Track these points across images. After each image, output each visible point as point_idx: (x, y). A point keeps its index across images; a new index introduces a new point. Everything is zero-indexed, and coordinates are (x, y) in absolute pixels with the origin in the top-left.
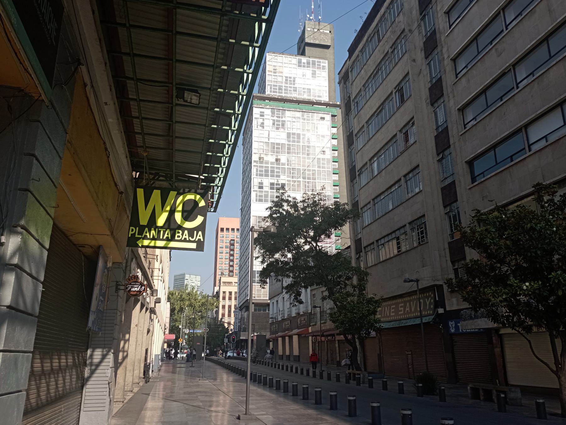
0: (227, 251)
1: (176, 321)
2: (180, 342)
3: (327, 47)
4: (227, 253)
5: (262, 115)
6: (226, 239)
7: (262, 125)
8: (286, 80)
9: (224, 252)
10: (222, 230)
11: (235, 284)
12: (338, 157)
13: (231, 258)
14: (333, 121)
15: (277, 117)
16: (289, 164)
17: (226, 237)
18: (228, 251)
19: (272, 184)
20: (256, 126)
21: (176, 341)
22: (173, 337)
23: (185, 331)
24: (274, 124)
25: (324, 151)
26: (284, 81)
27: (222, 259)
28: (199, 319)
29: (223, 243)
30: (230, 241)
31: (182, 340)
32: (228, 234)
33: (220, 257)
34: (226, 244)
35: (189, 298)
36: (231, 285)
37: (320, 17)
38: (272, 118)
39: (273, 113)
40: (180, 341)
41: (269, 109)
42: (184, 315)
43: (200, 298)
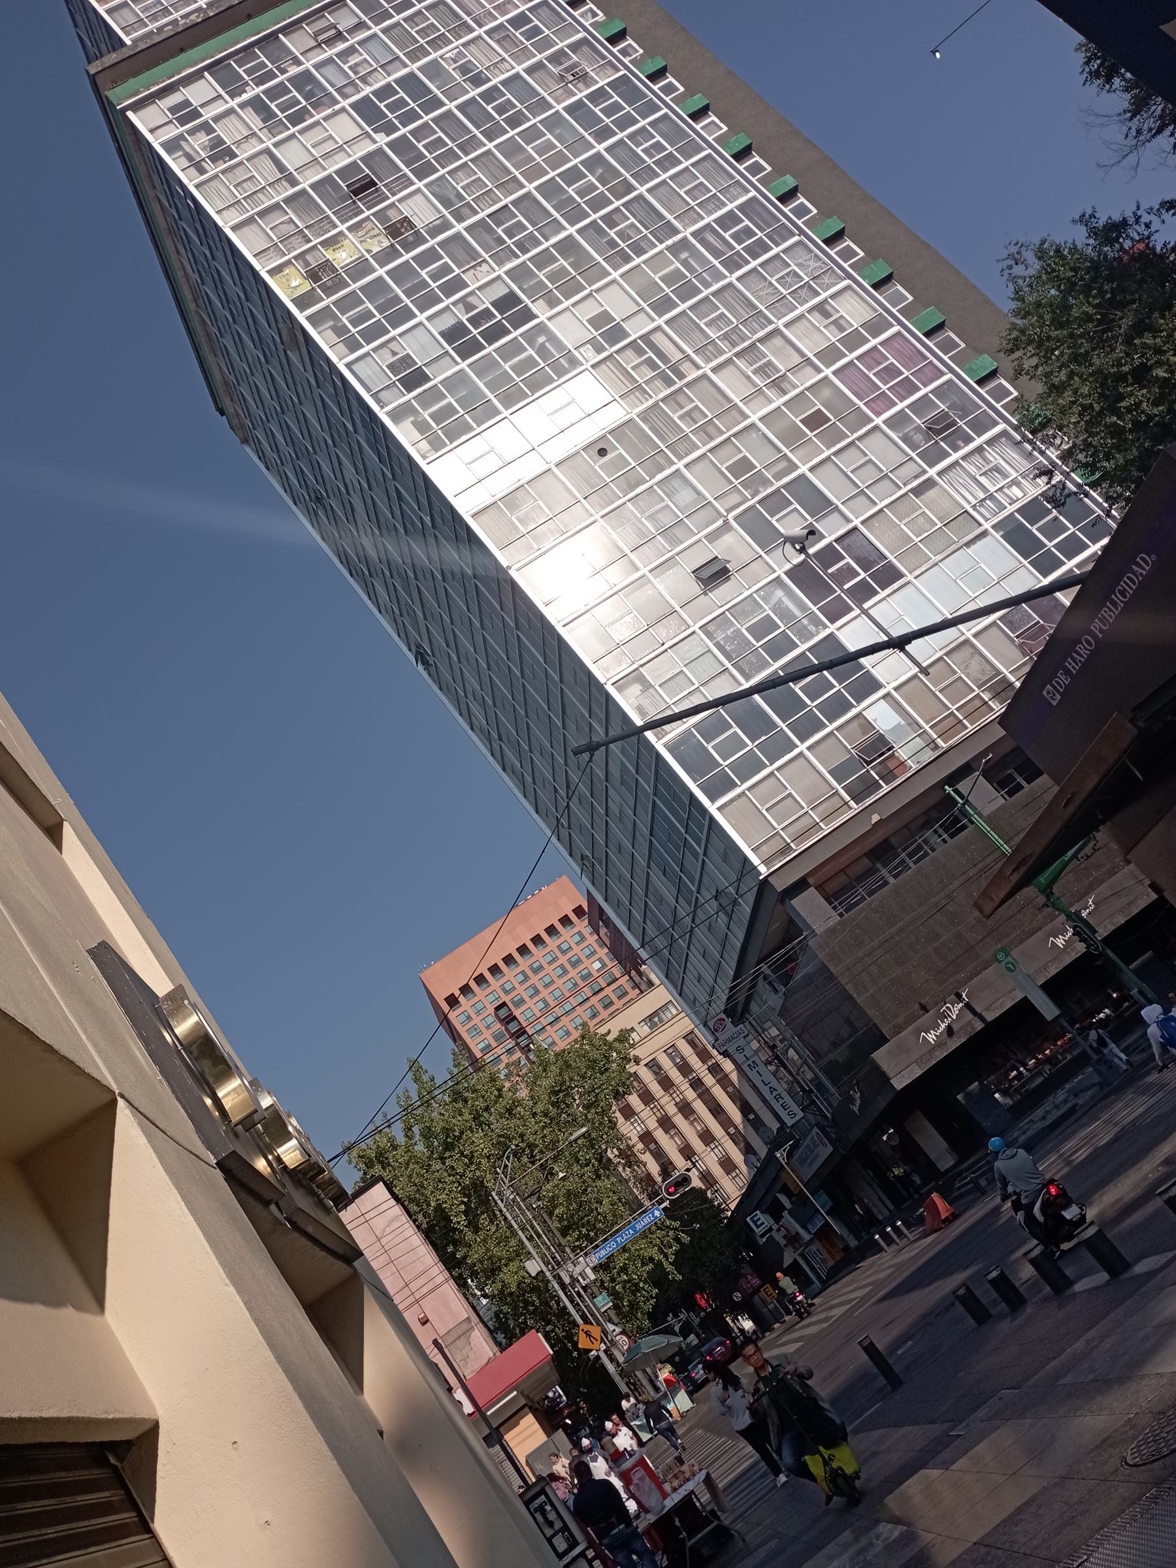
2: (598, 1350)
5: (186, 114)
6: (481, 1017)
7: (221, 152)
10: (452, 1001)
15: (259, 82)
17: (478, 1013)
19: (453, 334)
29: (480, 1033)
30: (496, 1015)
31: (596, 1331)
34: (491, 1031)
39: (233, 86)
40: (590, 1342)
42: (507, 1193)
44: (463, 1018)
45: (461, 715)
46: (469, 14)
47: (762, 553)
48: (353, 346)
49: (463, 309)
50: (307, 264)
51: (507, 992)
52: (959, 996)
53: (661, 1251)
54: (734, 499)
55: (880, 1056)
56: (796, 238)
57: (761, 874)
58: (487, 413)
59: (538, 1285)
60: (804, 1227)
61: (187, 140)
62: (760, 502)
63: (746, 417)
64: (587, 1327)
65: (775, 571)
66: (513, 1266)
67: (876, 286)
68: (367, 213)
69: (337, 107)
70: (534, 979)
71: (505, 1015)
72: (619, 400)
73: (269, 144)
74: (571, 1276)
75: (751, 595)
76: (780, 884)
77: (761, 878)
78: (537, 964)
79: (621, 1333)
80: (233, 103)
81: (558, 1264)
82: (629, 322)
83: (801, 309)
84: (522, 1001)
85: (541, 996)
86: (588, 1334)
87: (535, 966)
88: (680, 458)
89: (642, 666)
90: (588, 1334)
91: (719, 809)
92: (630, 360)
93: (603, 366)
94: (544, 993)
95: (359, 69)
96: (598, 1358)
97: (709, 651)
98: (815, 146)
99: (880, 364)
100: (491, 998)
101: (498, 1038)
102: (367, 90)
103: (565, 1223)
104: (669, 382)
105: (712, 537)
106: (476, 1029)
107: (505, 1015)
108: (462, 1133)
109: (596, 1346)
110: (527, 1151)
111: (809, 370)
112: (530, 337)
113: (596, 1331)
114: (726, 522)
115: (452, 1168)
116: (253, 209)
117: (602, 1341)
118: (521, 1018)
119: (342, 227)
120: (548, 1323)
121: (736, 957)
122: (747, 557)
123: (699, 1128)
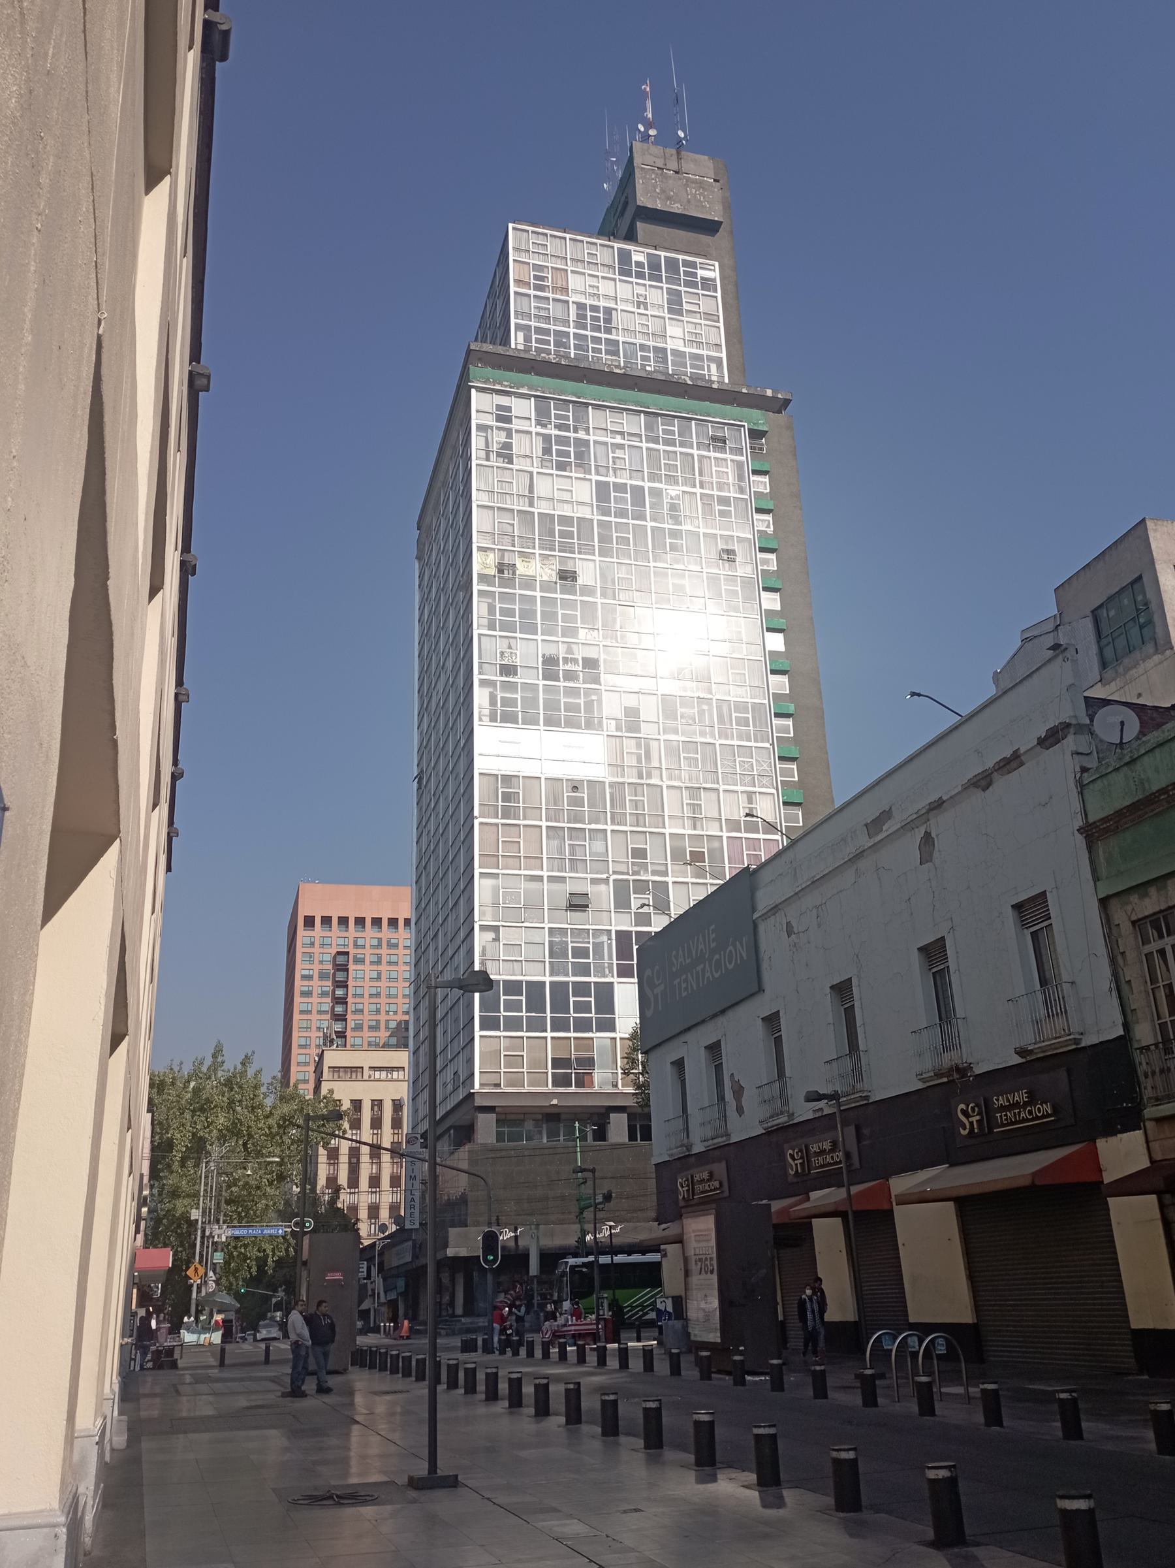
0: (325, 989)
1: (175, 1194)
2: (195, 1281)
3: (710, 227)
4: (324, 994)
5: (504, 416)
6: (322, 950)
7: (506, 453)
8: (581, 316)
9: (317, 991)
10: (309, 922)
11: (372, 1073)
12: (778, 573)
13: (339, 1009)
14: (756, 452)
15: (559, 427)
16: (610, 592)
17: (322, 945)
18: (327, 989)
20: (483, 454)
21: (176, 1278)
22: (165, 1258)
23: (217, 1232)
24: (547, 451)
25: (729, 552)
26: (572, 317)
27: (309, 1012)
28: (271, 1183)
29: (311, 962)
31: (201, 1271)
32: (328, 934)
33: (304, 1007)
34: (321, 967)
35: (231, 1102)
36: (359, 1077)
37: (681, 134)
38: (539, 429)
39: (542, 417)
40: (194, 1276)
41: (528, 397)
43: (269, 1102)
44: (307, 940)
45: (417, 829)
46: (701, 474)
47: (613, 910)
48: (492, 627)
49: (565, 650)
50: (502, 557)
51: (356, 945)
52: (516, 1230)
53: (273, 1250)
54: (623, 868)
55: (453, 1232)
56: (767, 745)
57: (473, 1089)
58: (530, 720)
59: (192, 1224)
60: (385, 1292)
61: (493, 431)
62: (634, 881)
63: (664, 827)
64: (198, 1266)
65: (611, 925)
66: (186, 1201)
67: (785, 803)
68: (556, 553)
69: (588, 477)
70: (384, 951)
71: (341, 963)
72: (607, 766)
73: (535, 470)
74: (211, 1233)
75: (589, 930)
76: (479, 1102)
77: (472, 1091)
78: (396, 941)
79: (213, 1281)
80: (534, 430)
81: (210, 1221)
82: (645, 724)
83: (739, 788)
84: (362, 961)
85: (380, 968)
86: (196, 1269)
87: (393, 941)
88: (613, 823)
89: (503, 926)
90: (196, 1269)
91: (481, 1036)
92: (630, 746)
93: (614, 739)
94: (384, 967)
95: (618, 461)
96: (192, 1285)
97: (544, 944)
98: (821, 697)
99: (755, 851)
100: (341, 941)
101: (323, 976)
102: (611, 479)
103: (234, 1198)
104: (640, 776)
105: (595, 881)
106: (311, 957)
107: (341, 963)
108: (215, 1107)
109: (195, 1279)
110: (246, 1138)
111: (717, 824)
112: (588, 692)
113: (201, 1271)
114: (607, 880)
115: (195, 1123)
116: (497, 503)
117: (201, 1278)
118: (352, 974)
119: (537, 551)
120: (182, 1245)
121: (456, 1102)
122: (605, 907)
123: (395, 1171)
